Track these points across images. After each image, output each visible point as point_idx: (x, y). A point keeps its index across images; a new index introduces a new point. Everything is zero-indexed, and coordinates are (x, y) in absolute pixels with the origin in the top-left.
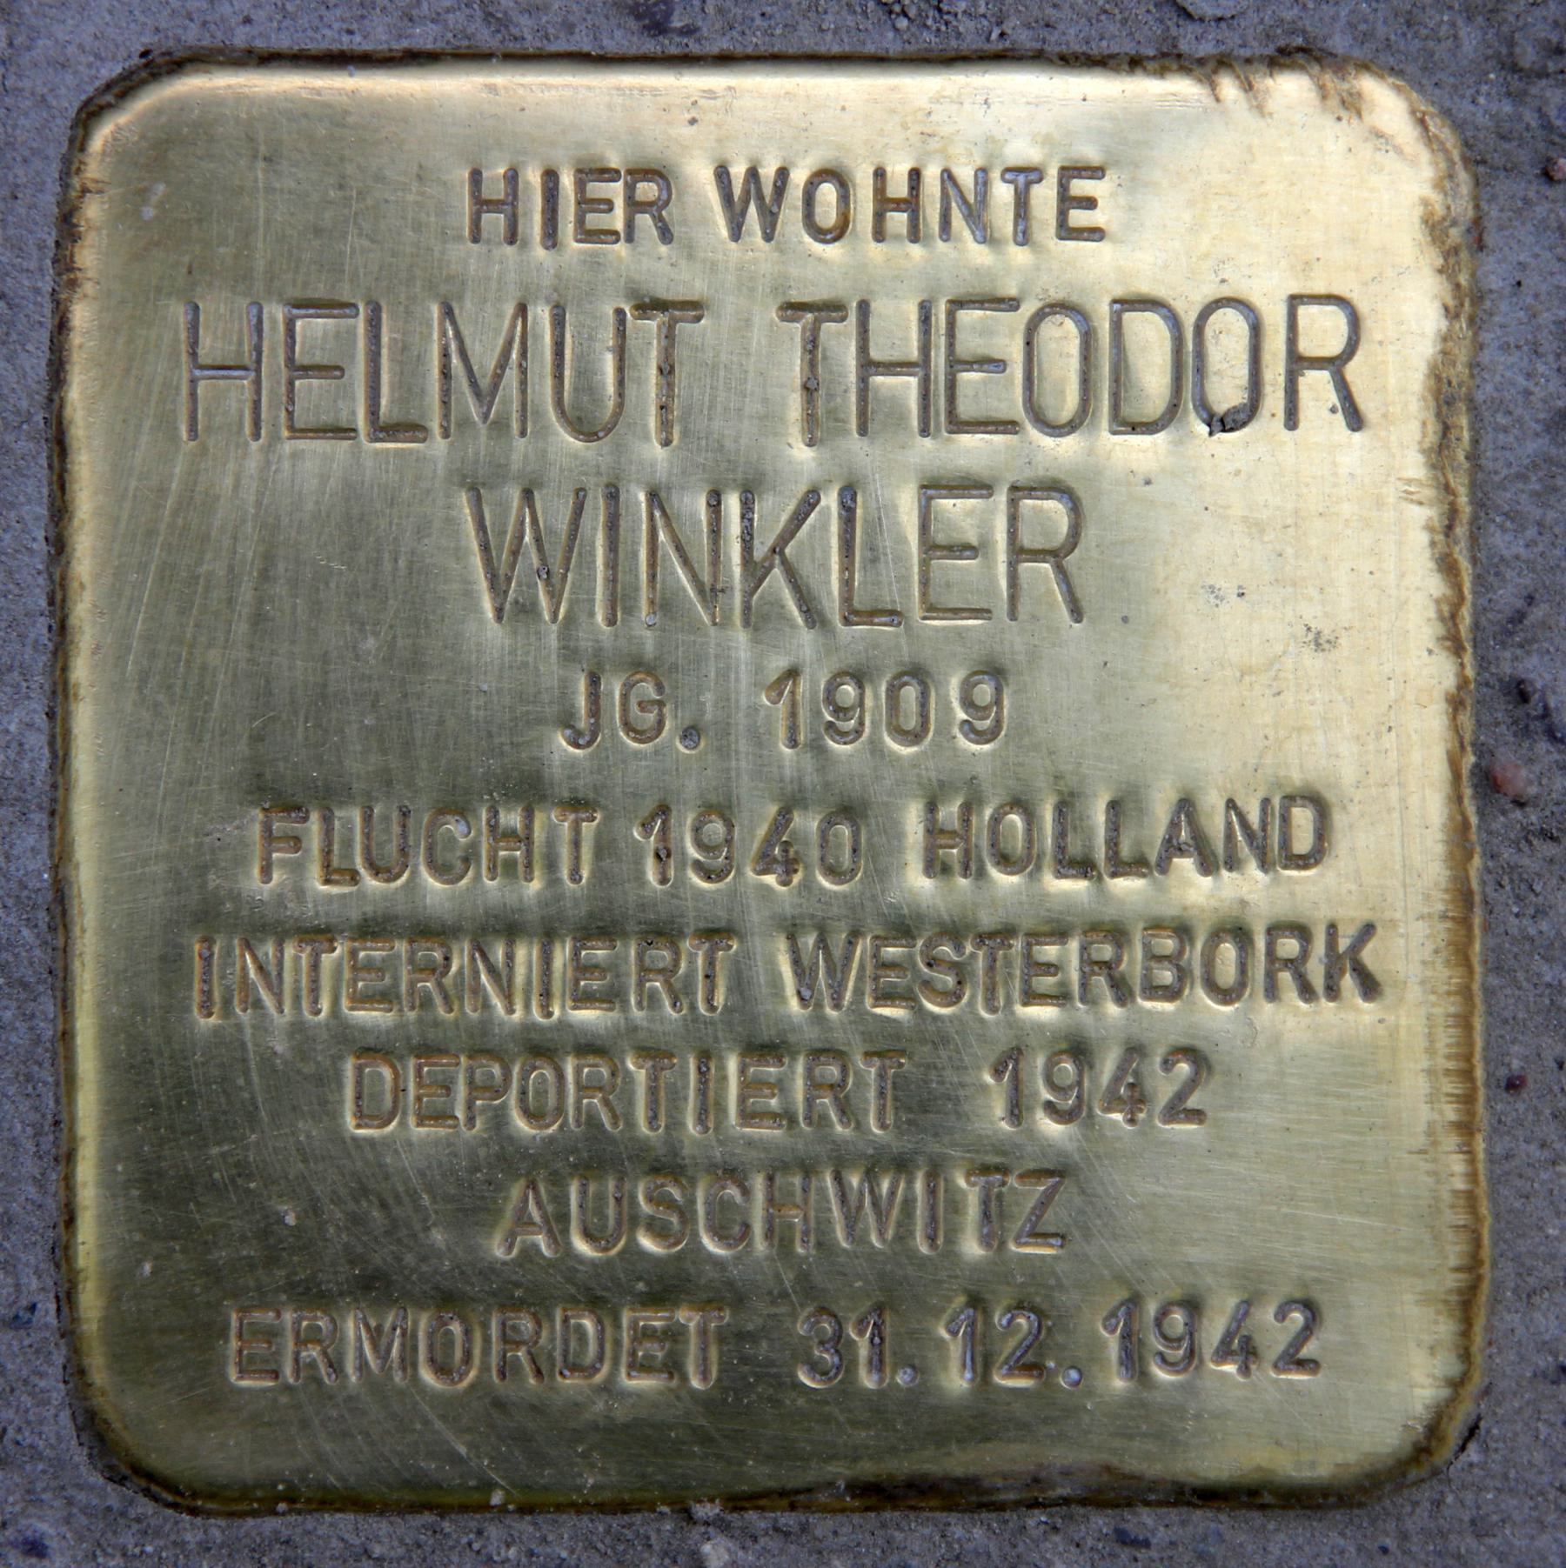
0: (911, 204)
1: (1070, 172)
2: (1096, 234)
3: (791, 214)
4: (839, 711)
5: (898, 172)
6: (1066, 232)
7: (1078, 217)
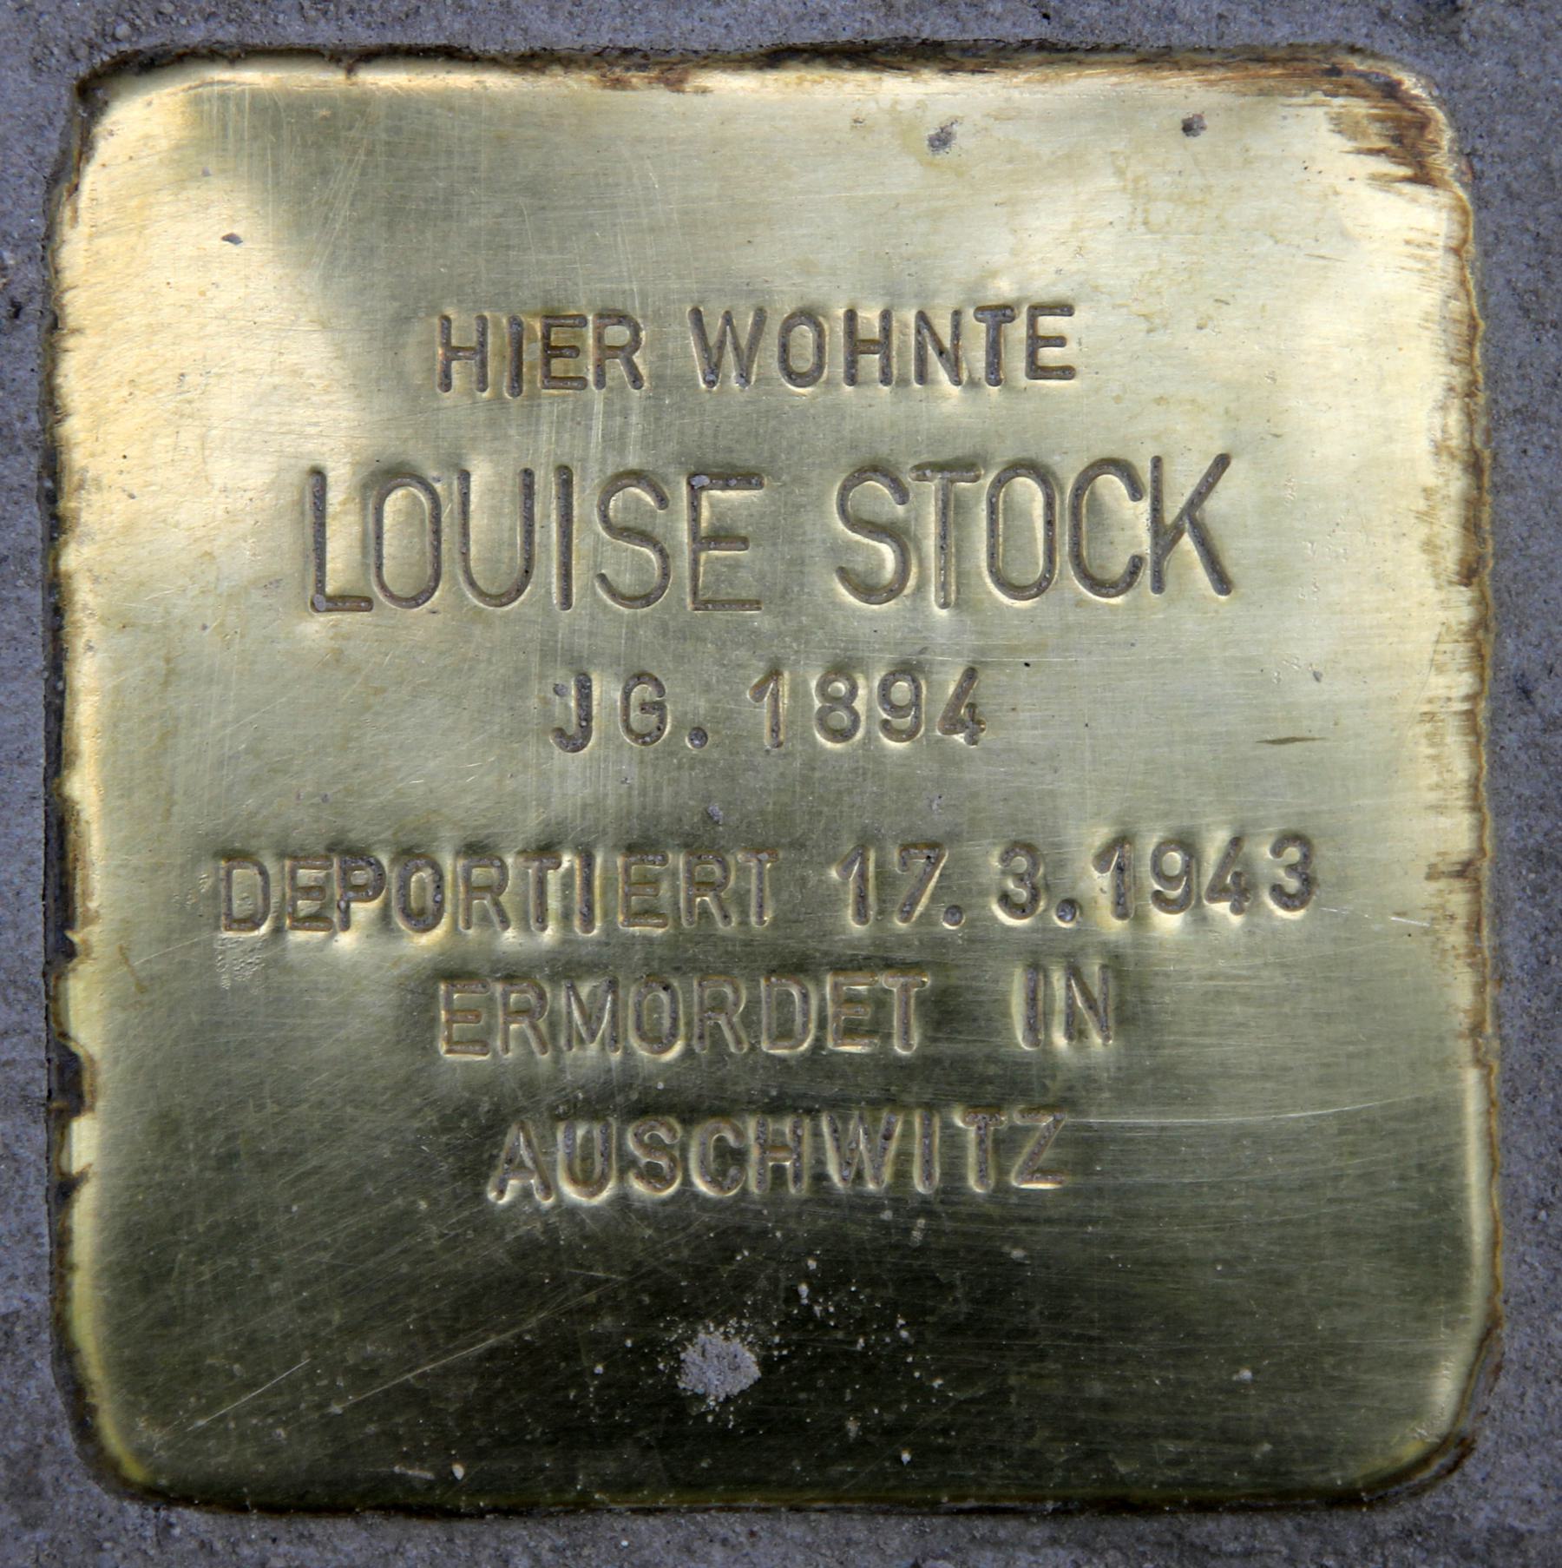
0: (883, 344)
1: (1038, 310)
2: (1066, 372)
3: (768, 359)
4: (894, 709)
5: (870, 317)
6: (1037, 371)
7: (1049, 355)
